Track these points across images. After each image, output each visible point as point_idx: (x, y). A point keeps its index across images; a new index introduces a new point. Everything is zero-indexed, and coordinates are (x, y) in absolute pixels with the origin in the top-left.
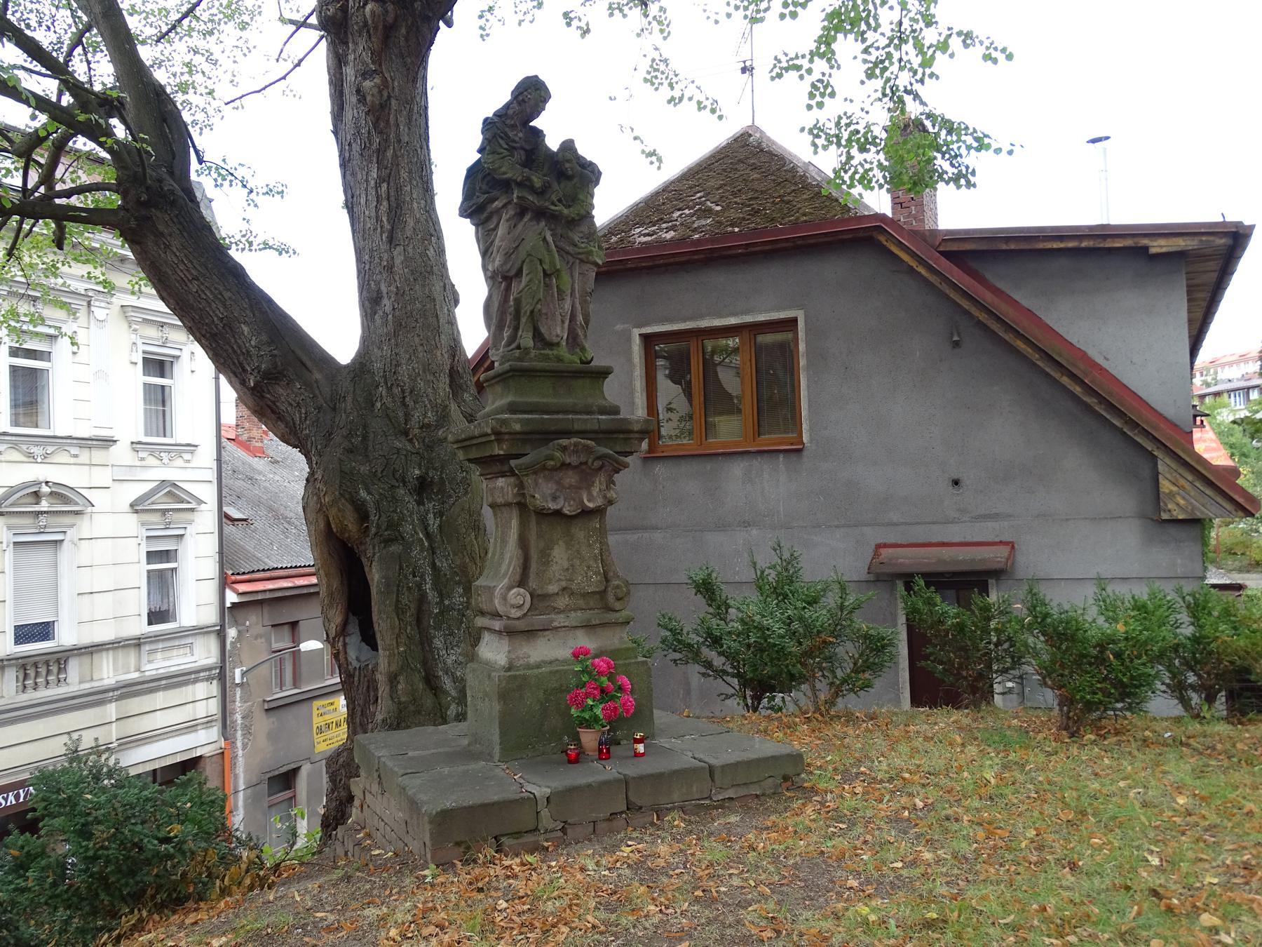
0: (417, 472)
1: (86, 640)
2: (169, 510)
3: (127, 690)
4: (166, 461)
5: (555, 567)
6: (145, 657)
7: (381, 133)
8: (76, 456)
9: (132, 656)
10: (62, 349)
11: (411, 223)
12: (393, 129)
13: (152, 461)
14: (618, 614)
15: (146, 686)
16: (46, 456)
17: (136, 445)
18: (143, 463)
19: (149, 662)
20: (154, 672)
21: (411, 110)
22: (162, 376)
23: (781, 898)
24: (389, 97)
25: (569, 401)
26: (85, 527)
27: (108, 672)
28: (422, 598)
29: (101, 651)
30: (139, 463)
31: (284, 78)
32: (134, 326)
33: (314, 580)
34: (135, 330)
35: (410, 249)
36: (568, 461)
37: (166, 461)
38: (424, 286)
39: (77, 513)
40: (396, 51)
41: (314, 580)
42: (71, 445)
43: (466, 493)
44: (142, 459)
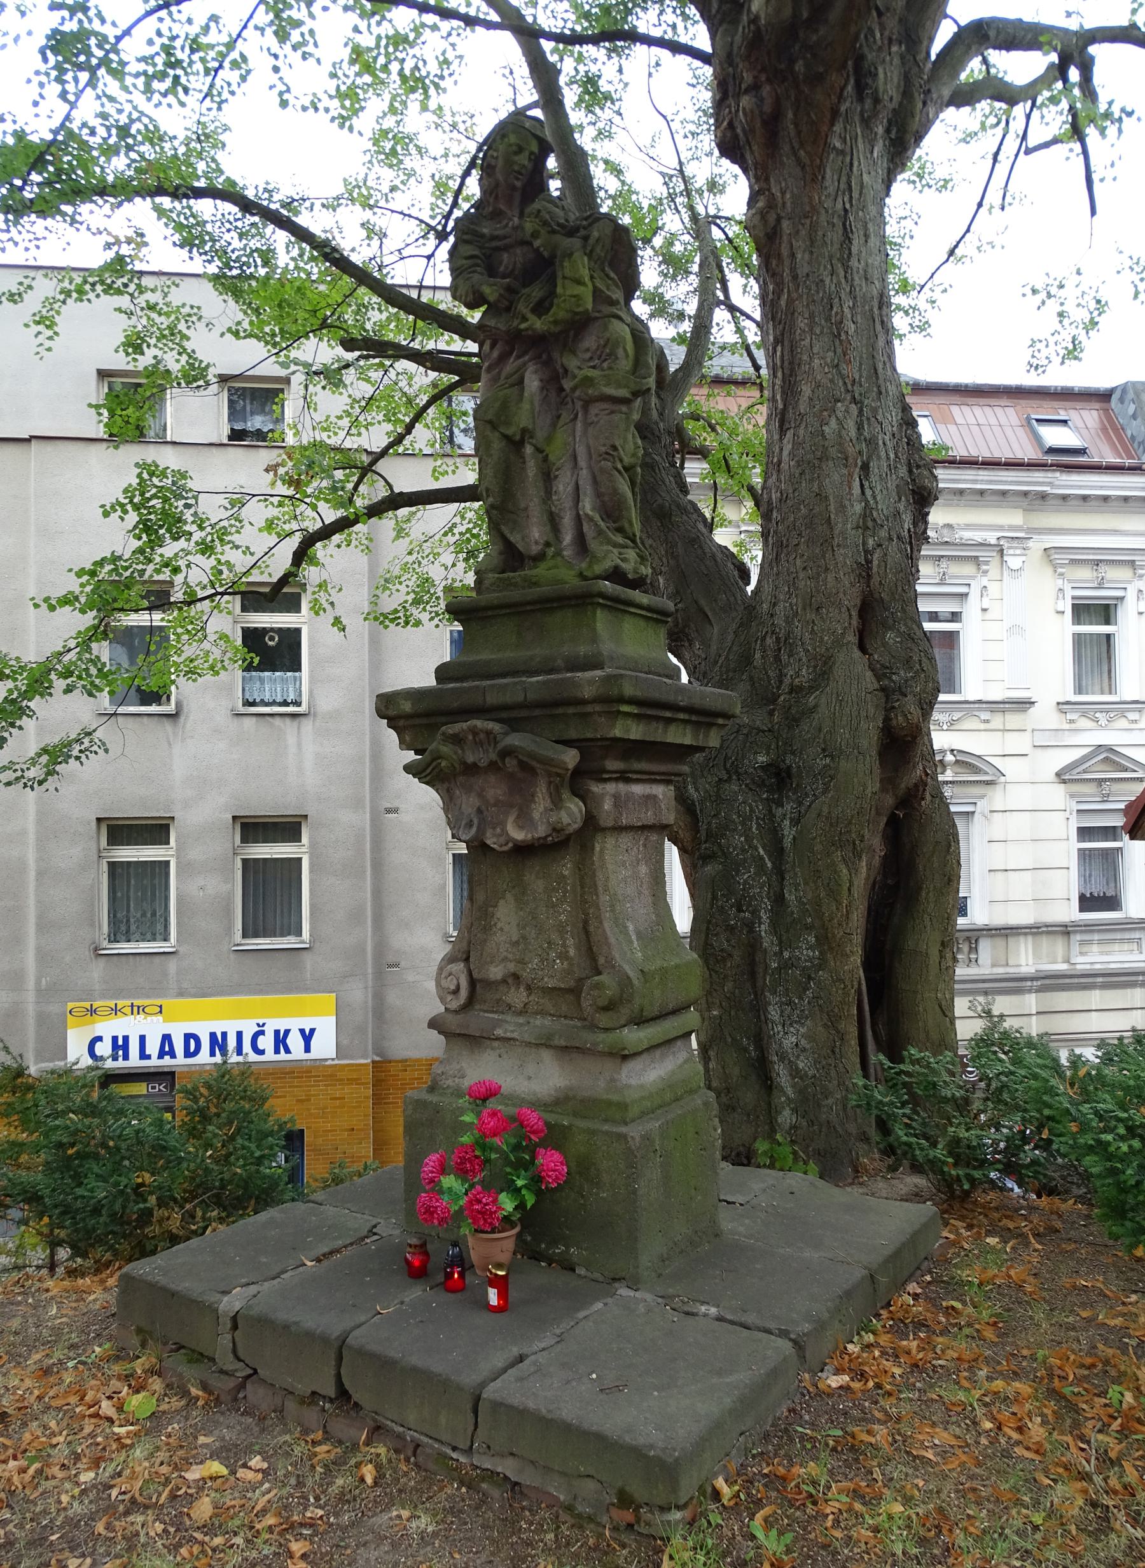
0: (762, 759)
1: (999, 920)
2: (1106, 780)
3: (1049, 982)
4: (1103, 722)
5: (500, 938)
6: (1075, 948)
8: (987, 721)
9: (1059, 945)
10: (971, 610)
11: (806, 390)
12: (787, 262)
13: (1084, 723)
14: (601, 1036)
15: (1076, 980)
16: (952, 723)
17: (1063, 706)
18: (1073, 726)
19: (1081, 953)
20: (1088, 967)
21: (813, 228)
22: (1107, 622)
24: (779, 220)
25: (538, 652)
26: (997, 799)
27: (1026, 959)
28: (753, 946)
29: (1019, 934)
30: (1067, 726)
31: (968, 231)
32: (1060, 570)
34: (1061, 574)
36: (470, 759)
37: (1103, 722)
38: (812, 480)
39: (988, 783)
40: (786, 148)
42: (980, 709)
43: (826, 791)
44: (1072, 721)
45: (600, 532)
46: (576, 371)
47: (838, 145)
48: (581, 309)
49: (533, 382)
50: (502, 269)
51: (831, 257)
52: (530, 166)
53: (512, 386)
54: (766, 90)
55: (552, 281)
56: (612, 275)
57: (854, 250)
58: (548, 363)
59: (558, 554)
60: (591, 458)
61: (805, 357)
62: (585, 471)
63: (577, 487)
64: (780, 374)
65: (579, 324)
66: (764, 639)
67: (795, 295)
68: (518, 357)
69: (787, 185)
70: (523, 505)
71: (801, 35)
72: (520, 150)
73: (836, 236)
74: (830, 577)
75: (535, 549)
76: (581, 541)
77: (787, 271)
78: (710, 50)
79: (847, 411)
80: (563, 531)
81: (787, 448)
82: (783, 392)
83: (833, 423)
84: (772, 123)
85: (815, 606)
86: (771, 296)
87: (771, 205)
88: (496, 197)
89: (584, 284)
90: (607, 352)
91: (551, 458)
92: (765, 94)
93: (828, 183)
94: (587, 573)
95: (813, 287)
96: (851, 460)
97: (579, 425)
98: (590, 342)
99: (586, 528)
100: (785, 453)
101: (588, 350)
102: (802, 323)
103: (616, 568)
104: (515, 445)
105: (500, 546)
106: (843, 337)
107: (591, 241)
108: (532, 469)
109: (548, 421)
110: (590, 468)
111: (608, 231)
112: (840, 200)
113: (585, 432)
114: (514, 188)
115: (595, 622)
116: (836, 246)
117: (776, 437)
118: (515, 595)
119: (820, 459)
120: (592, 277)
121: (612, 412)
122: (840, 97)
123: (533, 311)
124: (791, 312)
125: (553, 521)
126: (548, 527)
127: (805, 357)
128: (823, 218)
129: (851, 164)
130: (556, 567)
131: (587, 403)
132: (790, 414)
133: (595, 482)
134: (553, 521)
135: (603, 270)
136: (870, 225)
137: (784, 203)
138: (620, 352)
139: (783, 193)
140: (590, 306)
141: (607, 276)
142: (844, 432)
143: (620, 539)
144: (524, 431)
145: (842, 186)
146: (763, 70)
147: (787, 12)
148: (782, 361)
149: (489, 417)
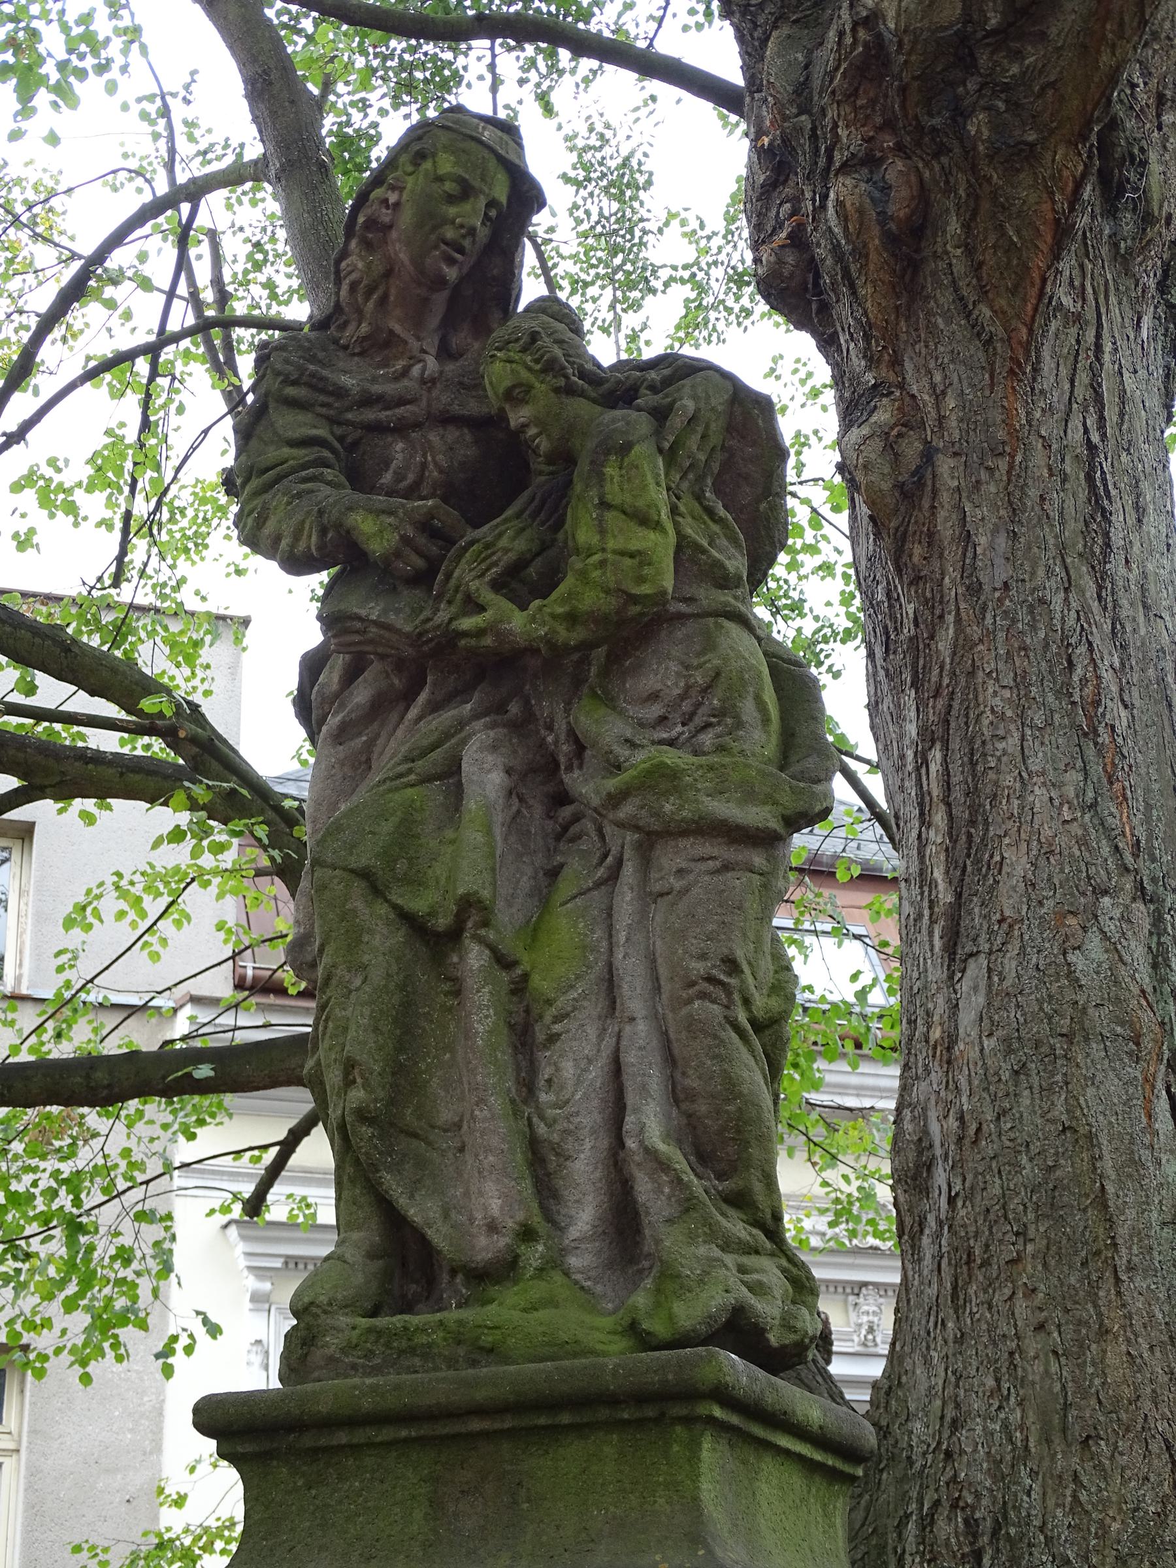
7: (917, 580)
11: (1017, 862)
12: (952, 554)
21: (1016, 480)
23: (482, 932)
24: (928, 455)
33: (309, 1029)
35: (1010, 965)
38: (1047, 1090)
40: (945, 298)
41: (309, 1029)
45: (688, 1205)
46: (623, 752)
47: (1067, 301)
48: (646, 589)
49: (486, 774)
50: (387, 478)
51: (1062, 550)
52: (483, 233)
53: (426, 779)
54: (895, 170)
55: (553, 511)
56: (722, 512)
57: (1117, 540)
58: (523, 726)
59: (554, 1263)
60: (657, 989)
61: (1008, 780)
62: (642, 1027)
63: (617, 1069)
64: (939, 818)
65: (632, 630)
66: (927, 1522)
67: (975, 632)
68: (434, 707)
69: (947, 375)
70: (446, 1115)
71: (983, 59)
72: (466, 191)
73: (1075, 500)
74: (1114, 1356)
75: (485, 1248)
76: (624, 1223)
77: (952, 575)
78: (737, 78)
79: (1126, 919)
80: (570, 1195)
81: (972, 1005)
82: (951, 863)
83: (1094, 944)
84: (908, 244)
85: (1077, 1432)
86: (908, 630)
87: (909, 419)
88: (383, 301)
89: (657, 526)
90: (707, 707)
91: (540, 983)
92: (891, 176)
93: (1046, 381)
94: (658, 1327)
95: (1023, 615)
96: (1147, 1043)
97: (626, 900)
98: (662, 673)
99: (644, 1188)
100: (967, 1018)
101: (654, 697)
102: (995, 698)
103: (739, 1312)
104: (434, 941)
105: (369, 1235)
106: (1104, 738)
107: (676, 422)
108: (484, 1011)
109: (525, 883)
110: (655, 1017)
111: (719, 401)
112: (1076, 422)
113: (643, 915)
114: (440, 282)
115: (695, 1477)
116: (1073, 526)
117: (936, 974)
118: (434, 1384)
119: (1068, 1037)
120: (674, 511)
121: (727, 867)
122: (1075, 198)
123: (497, 586)
124: (969, 673)
125: (541, 1164)
126: (527, 1185)
127: (1008, 780)
128: (1039, 458)
129: (1098, 347)
130: (551, 1302)
131: (650, 840)
132: (975, 917)
133: (670, 1059)
134: (541, 1164)
135: (699, 497)
136: (1145, 485)
137: (941, 419)
138: (748, 709)
139: (939, 397)
140: (668, 583)
141: (710, 512)
142: (1123, 971)
143: (737, 1227)
144: (468, 904)
145: (1080, 392)
146: (888, 125)
147: (951, 11)
148: (948, 787)
149: (364, 858)
